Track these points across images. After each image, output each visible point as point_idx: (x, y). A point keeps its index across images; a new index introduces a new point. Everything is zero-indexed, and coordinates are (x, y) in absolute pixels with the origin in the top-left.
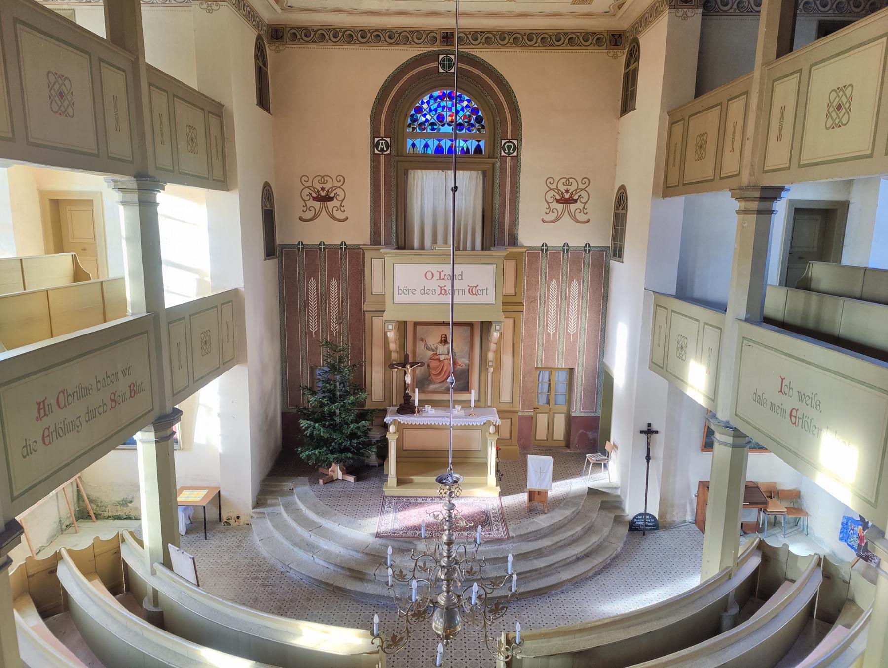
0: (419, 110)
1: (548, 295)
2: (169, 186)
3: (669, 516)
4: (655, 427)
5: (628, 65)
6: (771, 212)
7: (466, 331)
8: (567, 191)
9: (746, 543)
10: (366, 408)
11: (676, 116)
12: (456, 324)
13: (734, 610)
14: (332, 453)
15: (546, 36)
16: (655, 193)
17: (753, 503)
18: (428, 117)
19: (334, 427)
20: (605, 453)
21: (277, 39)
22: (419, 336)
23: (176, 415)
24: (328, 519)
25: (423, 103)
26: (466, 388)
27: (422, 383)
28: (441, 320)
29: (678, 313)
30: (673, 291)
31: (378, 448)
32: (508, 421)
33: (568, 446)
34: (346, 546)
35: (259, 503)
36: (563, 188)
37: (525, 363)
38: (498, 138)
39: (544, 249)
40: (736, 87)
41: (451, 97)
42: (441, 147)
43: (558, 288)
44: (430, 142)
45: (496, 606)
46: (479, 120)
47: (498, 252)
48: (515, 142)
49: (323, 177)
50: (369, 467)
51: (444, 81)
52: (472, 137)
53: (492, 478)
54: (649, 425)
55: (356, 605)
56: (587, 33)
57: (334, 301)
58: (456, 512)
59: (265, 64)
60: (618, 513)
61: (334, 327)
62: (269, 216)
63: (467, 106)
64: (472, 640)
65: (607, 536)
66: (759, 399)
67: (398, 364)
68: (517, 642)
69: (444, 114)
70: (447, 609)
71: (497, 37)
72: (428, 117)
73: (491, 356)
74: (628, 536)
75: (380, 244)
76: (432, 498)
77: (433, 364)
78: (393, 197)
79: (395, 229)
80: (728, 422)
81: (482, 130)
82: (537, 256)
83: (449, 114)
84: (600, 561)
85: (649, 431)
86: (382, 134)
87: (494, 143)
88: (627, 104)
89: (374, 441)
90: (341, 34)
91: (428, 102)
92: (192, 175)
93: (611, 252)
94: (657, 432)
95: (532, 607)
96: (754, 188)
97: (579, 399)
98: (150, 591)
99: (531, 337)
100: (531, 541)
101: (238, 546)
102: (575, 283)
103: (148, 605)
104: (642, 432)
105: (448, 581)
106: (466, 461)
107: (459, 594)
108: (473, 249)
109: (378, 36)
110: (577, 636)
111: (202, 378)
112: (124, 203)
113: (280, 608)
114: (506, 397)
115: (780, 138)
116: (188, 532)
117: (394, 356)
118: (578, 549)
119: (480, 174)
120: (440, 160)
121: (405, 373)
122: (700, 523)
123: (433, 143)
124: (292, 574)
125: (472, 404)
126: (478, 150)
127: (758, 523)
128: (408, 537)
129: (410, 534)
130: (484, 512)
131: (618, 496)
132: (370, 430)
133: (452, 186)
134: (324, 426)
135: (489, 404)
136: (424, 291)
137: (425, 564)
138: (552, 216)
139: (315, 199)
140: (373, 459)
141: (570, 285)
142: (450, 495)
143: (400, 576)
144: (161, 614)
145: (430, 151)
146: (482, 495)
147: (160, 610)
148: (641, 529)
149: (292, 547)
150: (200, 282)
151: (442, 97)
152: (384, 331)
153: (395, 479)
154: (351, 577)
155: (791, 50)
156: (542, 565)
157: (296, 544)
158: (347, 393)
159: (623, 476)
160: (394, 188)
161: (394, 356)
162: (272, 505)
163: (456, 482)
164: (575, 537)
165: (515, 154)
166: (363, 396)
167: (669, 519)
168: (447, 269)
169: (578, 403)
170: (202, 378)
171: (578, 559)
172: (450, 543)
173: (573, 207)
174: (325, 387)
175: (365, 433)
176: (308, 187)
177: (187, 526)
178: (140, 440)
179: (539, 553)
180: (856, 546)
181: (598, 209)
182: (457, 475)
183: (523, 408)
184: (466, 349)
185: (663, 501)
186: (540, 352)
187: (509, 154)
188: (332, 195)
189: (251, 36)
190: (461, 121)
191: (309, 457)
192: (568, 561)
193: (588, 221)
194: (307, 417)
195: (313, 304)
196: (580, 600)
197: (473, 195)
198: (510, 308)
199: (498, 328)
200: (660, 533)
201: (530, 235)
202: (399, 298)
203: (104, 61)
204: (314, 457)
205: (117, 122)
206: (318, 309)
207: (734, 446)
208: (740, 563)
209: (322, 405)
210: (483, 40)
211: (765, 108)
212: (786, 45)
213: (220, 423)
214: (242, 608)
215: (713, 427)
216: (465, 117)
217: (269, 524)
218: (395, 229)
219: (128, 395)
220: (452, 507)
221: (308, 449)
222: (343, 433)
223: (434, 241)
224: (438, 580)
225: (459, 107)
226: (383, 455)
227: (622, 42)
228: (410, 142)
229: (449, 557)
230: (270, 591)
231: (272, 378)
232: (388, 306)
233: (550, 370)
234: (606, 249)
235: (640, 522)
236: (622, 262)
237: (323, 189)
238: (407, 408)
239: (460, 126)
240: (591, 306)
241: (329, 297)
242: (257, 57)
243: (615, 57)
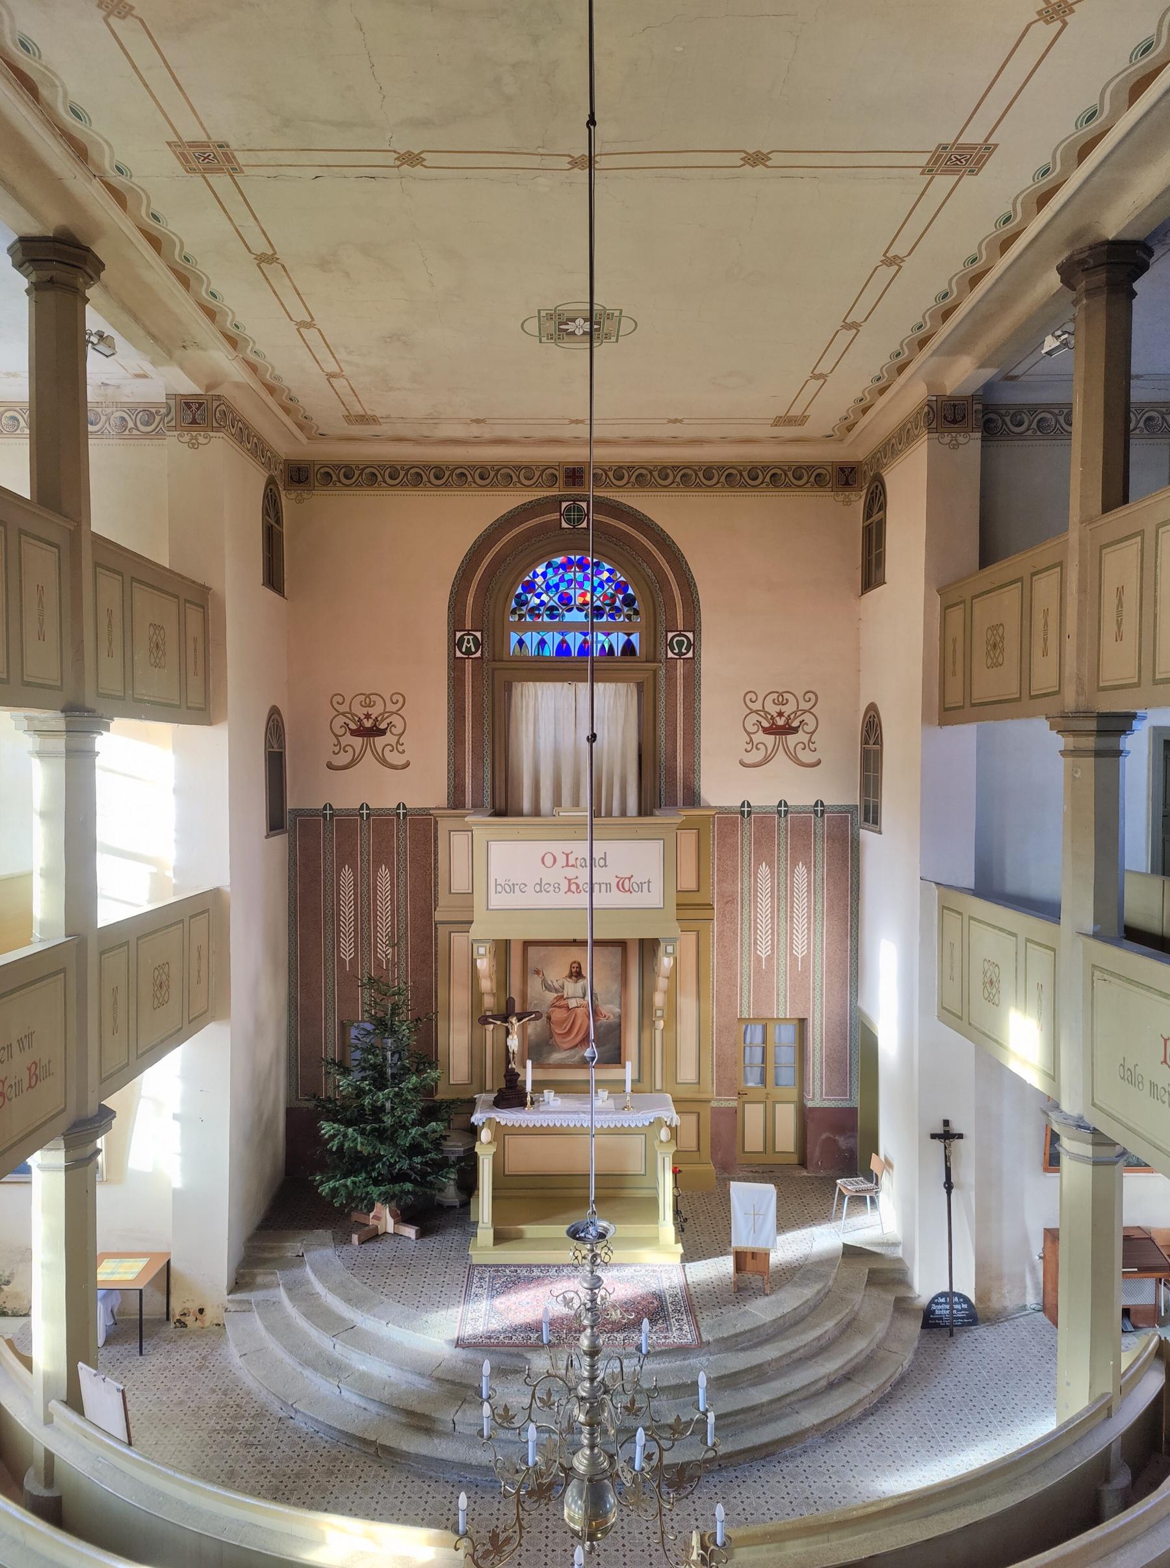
0: (530, 587)
1: (756, 891)
2: (117, 723)
3: (994, 1297)
4: (956, 1128)
5: (868, 514)
6: (1118, 753)
9: (1135, 1348)
10: (438, 1097)
11: (950, 596)
12: (597, 943)
13: (1122, 1479)
14: (376, 1183)
15: (734, 471)
16: (926, 718)
17: (1145, 1270)
19: (381, 1135)
20: (870, 1176)
21: (299, 482)
22: (531, 965)
23: (104, 1117)
24: (368, 1311)
25: (535, 575)
26: (615, 1058)
27: (537, 1050)
28: (571, 937)
29: (980, 922)
30: (970, 882)
31: (461, 1172)
32: (694, 1117)
33: (803, 1164)
34: (400, 1365)
35: (240, 1282)
36: (773, 710)
37: (719, 1011)
38: (661, 628)
39: (745, 811)
40: (1042, 554)
41: (582, 565)
42: (568, 646)
43: (772, 877)
44: (548, 637)
45: (680, 1479)
46: (629, 601)
47: (664, 818)
48: (690, 635)
49: (368, 696)
50: (443, 1210)
51: (574, 541)
52: (618, 627)
53: (667, 1227)
54: (946, 1123)
55: (418, 1482)
56: (800, 467)
57: (384, 907)
58: (602, 1292)
59: (279, 521)
60: (901, 1292)
61: (384, 951)
62: (275, 764)
63: (609, 580)
64: (637, 1550)
65: (884, 1339)
67: (494, 1017)
68: (719, 1542)
69: (571, 592)
70: (590, 1480)
71: (655, 474)
72: (544, 598)
73: (659, 999)
74: (922, 1337)
75: (463, 807)
76: (559, 1267)
77: (558, 1015)
78: (487, 727)
79: (492, 785)
80: (1081, 1118)
81: (634, 618)
82: (734, 823)
83: (579, 592)
84: (873, 1387)
86: (468, 626)
87: (657, 641)
88: (872, 573)
89: (453, 1158)
90: (402, 473)
91: (544, 575)
92: (154, 703)
93: (860, 816)
94: (960, 1136)
95: (750, 1482)
96: (1085, 714)
97: (818, 1074)
98: (40, 1455)
99: (728, 964)
100: (743, 1349)
101: (200, 1368)
102: (801, 869)
103: (33, 1485)
104: (933, 1136)
105: (591, 1425)
106: (618, 1193)
107: (613, 1451)
108: (623, 814)
109: (463, 474)
110: (833, 1536)
111: (152, 1048)
112: (41, 754)
113: (277, 1489)
114: (687, 1072)
115: (1119, 637)
116: (107, 1342)
117: (488, 1002)
118: (830, 1366)
120: (563, 665)
121: (508, 1033)
122: (1049, 1309)
123: (553, 640)
124: (299, 1421)
125: (628, 1087)
126: (628, 649)
127: (1157, 1307)
128: (515, 1345)
129: (518, 1338)
130: (654, 1294)
131: (899, 1260)
132: (444, 1138)
133: (588, 733)
134: (362, 1132)
135: (658, 1086)
136: (541, 887)
137: (549, 1394)
138: (756, 756)
139: (354, 733)
140: (450, 1194)
141: (793, 872)
142: (593, 1263)
143: (505, 1417)
144: (58, 1502)
145: (549, 651)
146: (651, 1261)
147: (57, 1494)
148: (944, 1323)
149: (300, 1369)
150: (157, 880)
152: (471, 959)
153: (492, 1231)
154: (409, 1426)
155: (1126, 500)
156: (765, 1398)
157: (307, 1363)
158: (406, 1071)
159: (907, 1220)
160: (487, 714)
161: (488, 1002)
162: (265, 1286)
163: (602, 1236)
164: (823, 1341)
165: (690, 655)
166: (434, 1075)
167: (995, 1303)
168: (580, 849)
169: (818, 1082)
170: (152, 1048)
171: (832, 1386)
172: (593, 1352)
173: (792, 739)
174: (365, 1060)
175: (437, 1144)
176: (343, 714)
177: (108, 1328)
178: (39, 1166)
179: (759, 1374)
181: (835, 743)
182: (605, 1224)
183: (718, 1094)
184: (615, 987)
185: (982, 1270)
186: (745, 989)
187: (680, 654)
188: (383, 726)
189: (257, 480)
190: (598, 603)
191: (334, 1191)
192: (813, 1389)
193: (819, 763)
194: (333, 1117)
195: (348, 911)
196: (838, 1466)
198: (690, 914)
199: (670, 949)
200: (980, 1331)
201: (724, 782)
202: (497, 900)
203: (27, 534)
204: (343, 1192)
205: (41, 626)
206: (356, 920)
207: (1096, 1163)
208: (1127, 1384)
209: (360, 1093)
210: (633, 479)
211: (1092, 589)
212: (1117, 493)
213: (179, 1130)
214: (209, 1487)
215: (1056, 1128)
216: (605, 596)
217: (259, 1324)
218: (492, 785)
219: (25, 1085)
220: (596, 1283)
221: (334, 1177)
222: (396, 1145)
223: (557, 802)
224: (572, 1428)
225: (596, 581)
226: (469, 1186)
227: (856, 480)
228: (514, 637)
229: (592, 1379)
230: (258, 1455)
231: (272, 1044)
232: (479, 914)
233: (766, 1023)
234: (851, 809)
235: (942, 1310)
236: (880, 832)
237: (368, 716)
238: (511, 1095)
239: (598, 612)
240: (831, 907)
241: (375, 900)
242: (266, 512)
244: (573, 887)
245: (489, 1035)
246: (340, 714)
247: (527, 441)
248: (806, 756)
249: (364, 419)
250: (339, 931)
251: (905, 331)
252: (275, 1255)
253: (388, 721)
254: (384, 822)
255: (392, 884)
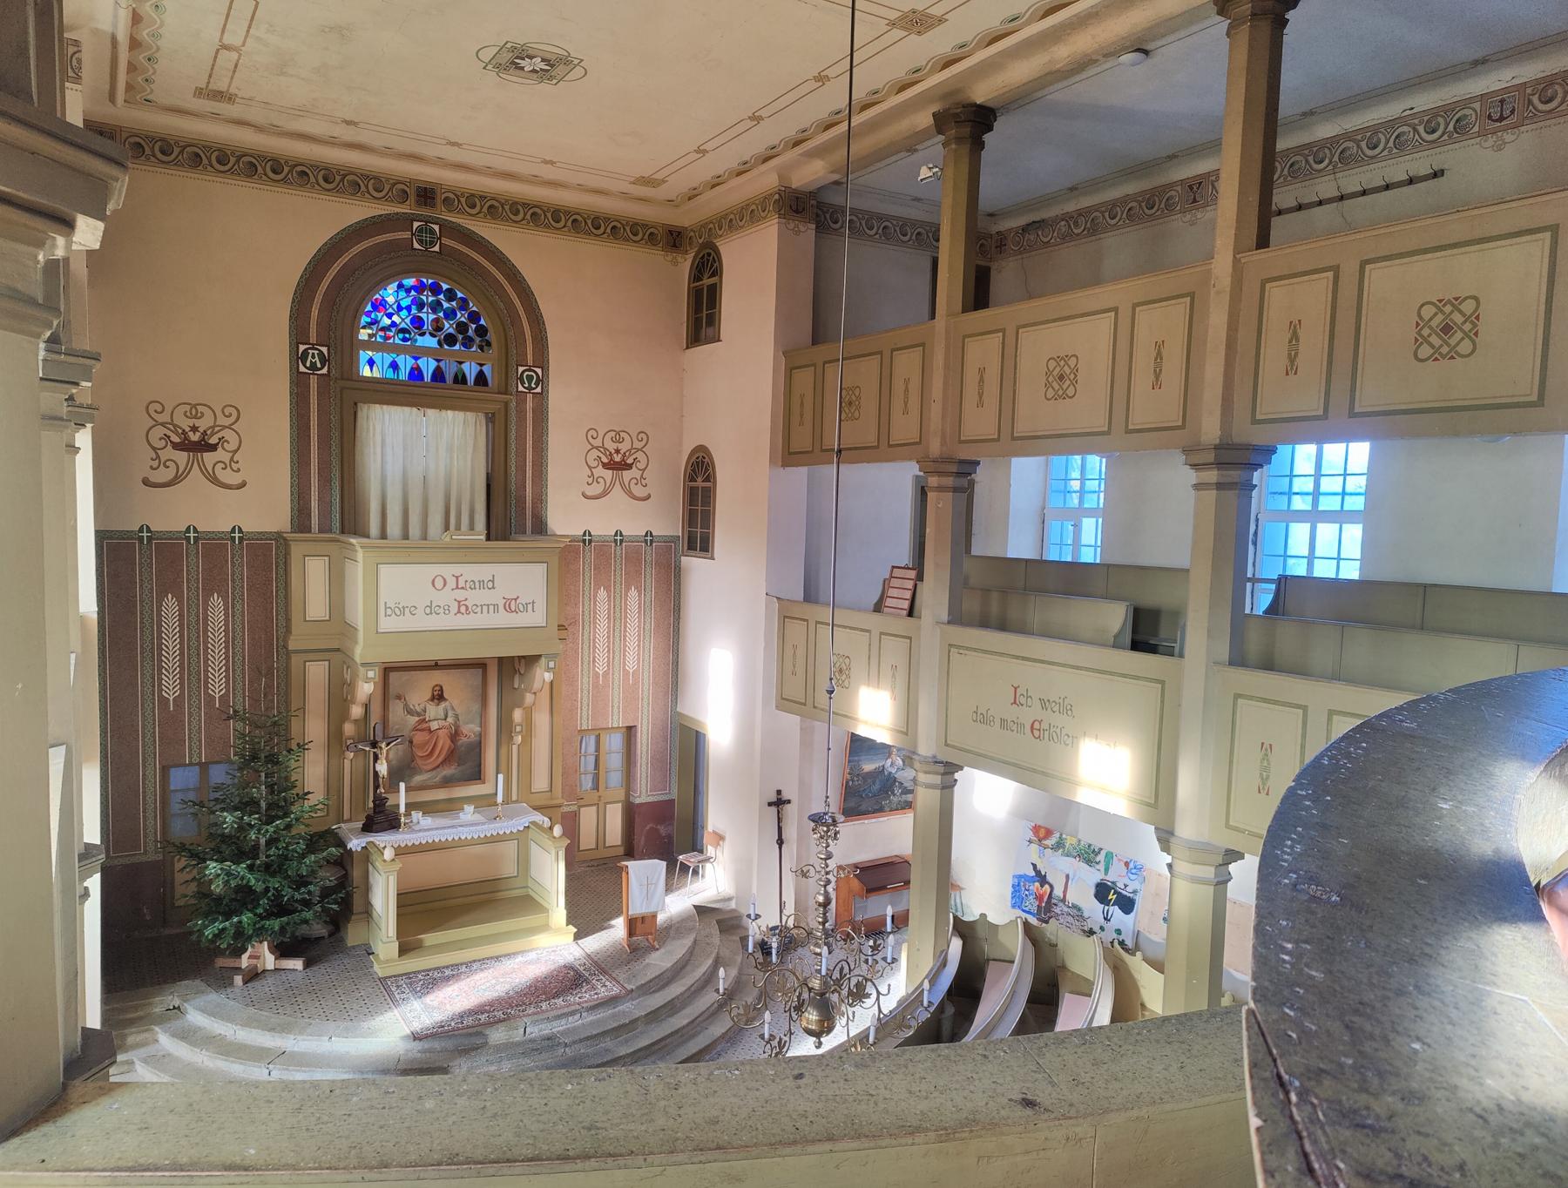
4: (785, 796)
7: (474, 676)
8: (618, 451)
11: (792, 362)
18: (395, 318)
22: (392, 691)
24: (301, 1033)
26: (477, 775)
36: (611, 446)
39: (587, 539)
42: (464, 376)
44: (400, 360)
48: (539, 371)
49: (195, 406)
54: (779, 792)
66: (983, 718)
69: (424, 316)
72: (395, 318)
75: (330, 531)
77: (419, 738)
78: (335, 450)
85: (779, 802)
86: (313, 340)
94: (789, 802)
102: (633, 593)
104: (770, 804)
119: (481, 416)
121: (376, 758)
123: (405, 363)
126: (481, 379)
129: (469, 1021)
136: (431, 609)
145: (403, 375)
146: (551, 944)
151: (420, 288)
156: (685, 1022)
160: (336, 434)
165: (539, 390)
173: (627, 475)
176: (163, 424)
179: (672, 1008)
180: (1034, 909)
184: (476, 707)
187: (530, 388)
193: (648, 497)
195: (171, 645)
197: (470, 450)
201: (568, 513)
234: (674, 539)
237: (194, 429)
238: (381, 819)
240: (657, 626)
241: (205, 631)
243: (675, 263)
244: (463, 609)
245: (347, 763)
246: (158, 424)
247: (388, 152)
248: (638, 491)
249: (218, 95)
250: (160, 668)
251: (791, 131)
252: (140, 1013)
253: (220, 435)
254: (215, 549)
255: (227, 615)
